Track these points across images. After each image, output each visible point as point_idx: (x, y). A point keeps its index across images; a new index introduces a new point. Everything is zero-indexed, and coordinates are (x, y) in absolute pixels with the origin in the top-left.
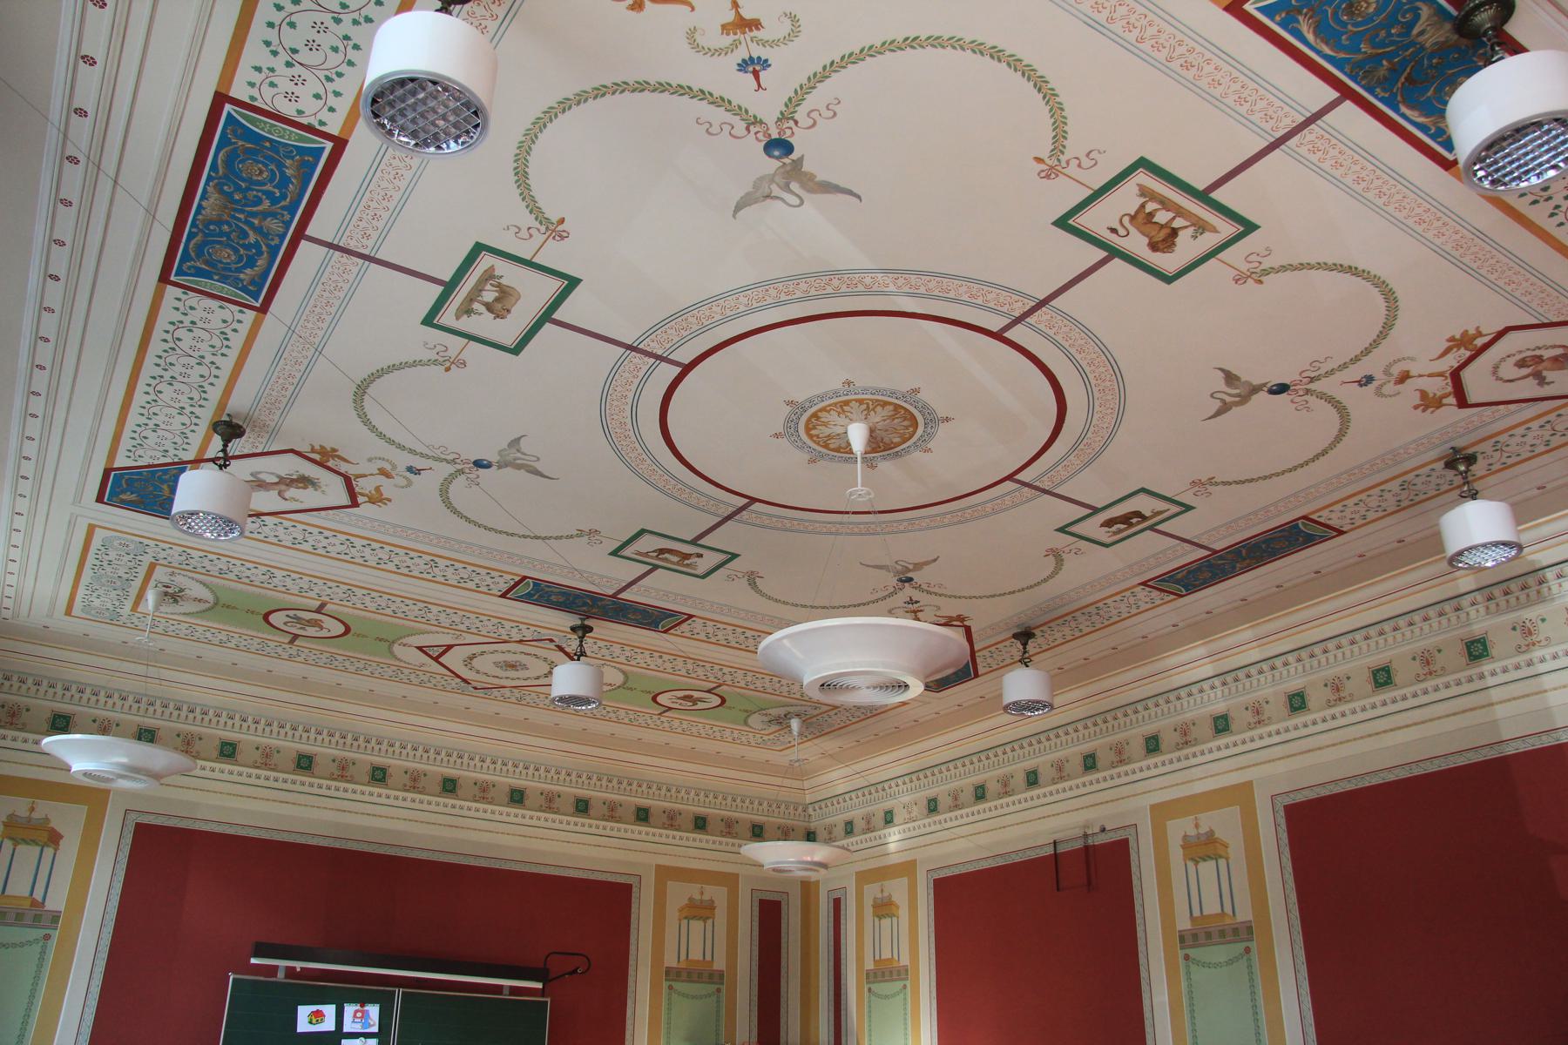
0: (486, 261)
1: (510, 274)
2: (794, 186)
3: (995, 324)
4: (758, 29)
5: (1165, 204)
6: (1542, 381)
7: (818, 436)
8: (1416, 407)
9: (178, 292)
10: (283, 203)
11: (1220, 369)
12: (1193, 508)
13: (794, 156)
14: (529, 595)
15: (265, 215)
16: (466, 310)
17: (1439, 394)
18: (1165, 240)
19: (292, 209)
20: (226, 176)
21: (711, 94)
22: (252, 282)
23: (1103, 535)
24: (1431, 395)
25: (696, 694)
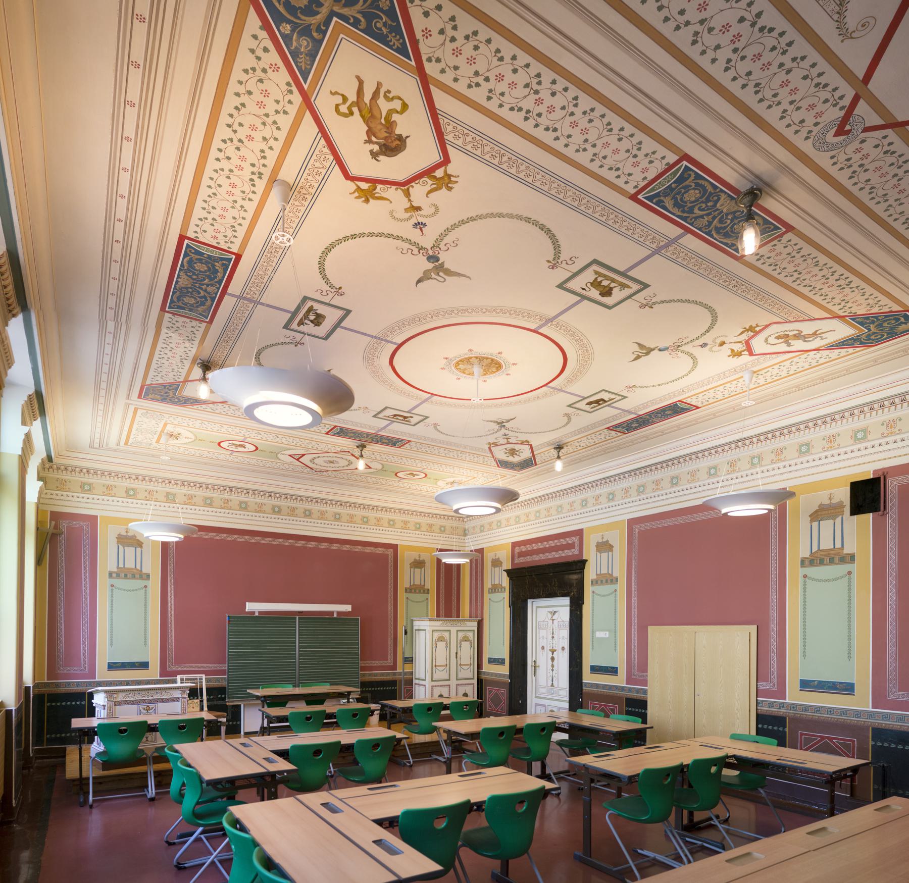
0: (309, 304)
1: (321, 309)
2: (441, 274)
3: (533, 326)
4: (420, 210)
5: (607, 278)
6: (789, 345)
7: (460, 369)
8: (729, 356)
9: (170, 315)
10: (216, 280)
11: (637, 343)
12: (627, 397)
13: (440, 262)
14: (338, 433)
15: (208, 285)
16: (301, 323)
17: (739, 350)
18: (607, 292)
19: (220, 282)
20: (188, 269)
21: (402, 237)
22: (204, 311)
23: (588, 408)
24: (736, 351)
25: (415, 473)
